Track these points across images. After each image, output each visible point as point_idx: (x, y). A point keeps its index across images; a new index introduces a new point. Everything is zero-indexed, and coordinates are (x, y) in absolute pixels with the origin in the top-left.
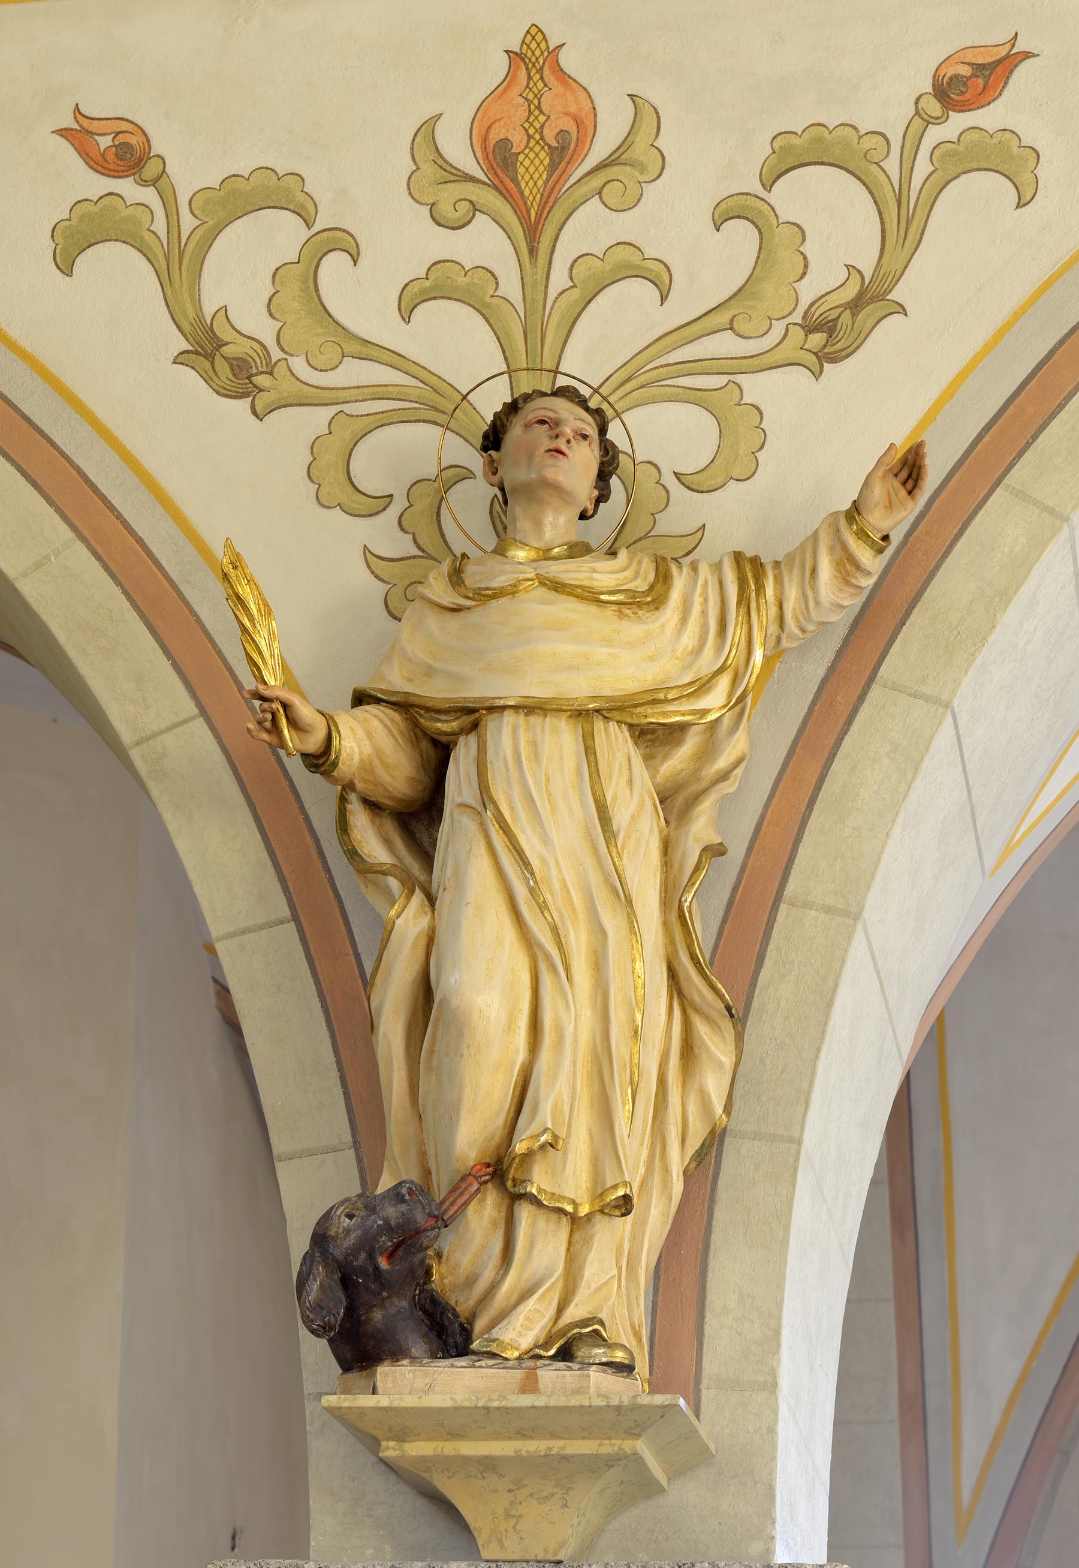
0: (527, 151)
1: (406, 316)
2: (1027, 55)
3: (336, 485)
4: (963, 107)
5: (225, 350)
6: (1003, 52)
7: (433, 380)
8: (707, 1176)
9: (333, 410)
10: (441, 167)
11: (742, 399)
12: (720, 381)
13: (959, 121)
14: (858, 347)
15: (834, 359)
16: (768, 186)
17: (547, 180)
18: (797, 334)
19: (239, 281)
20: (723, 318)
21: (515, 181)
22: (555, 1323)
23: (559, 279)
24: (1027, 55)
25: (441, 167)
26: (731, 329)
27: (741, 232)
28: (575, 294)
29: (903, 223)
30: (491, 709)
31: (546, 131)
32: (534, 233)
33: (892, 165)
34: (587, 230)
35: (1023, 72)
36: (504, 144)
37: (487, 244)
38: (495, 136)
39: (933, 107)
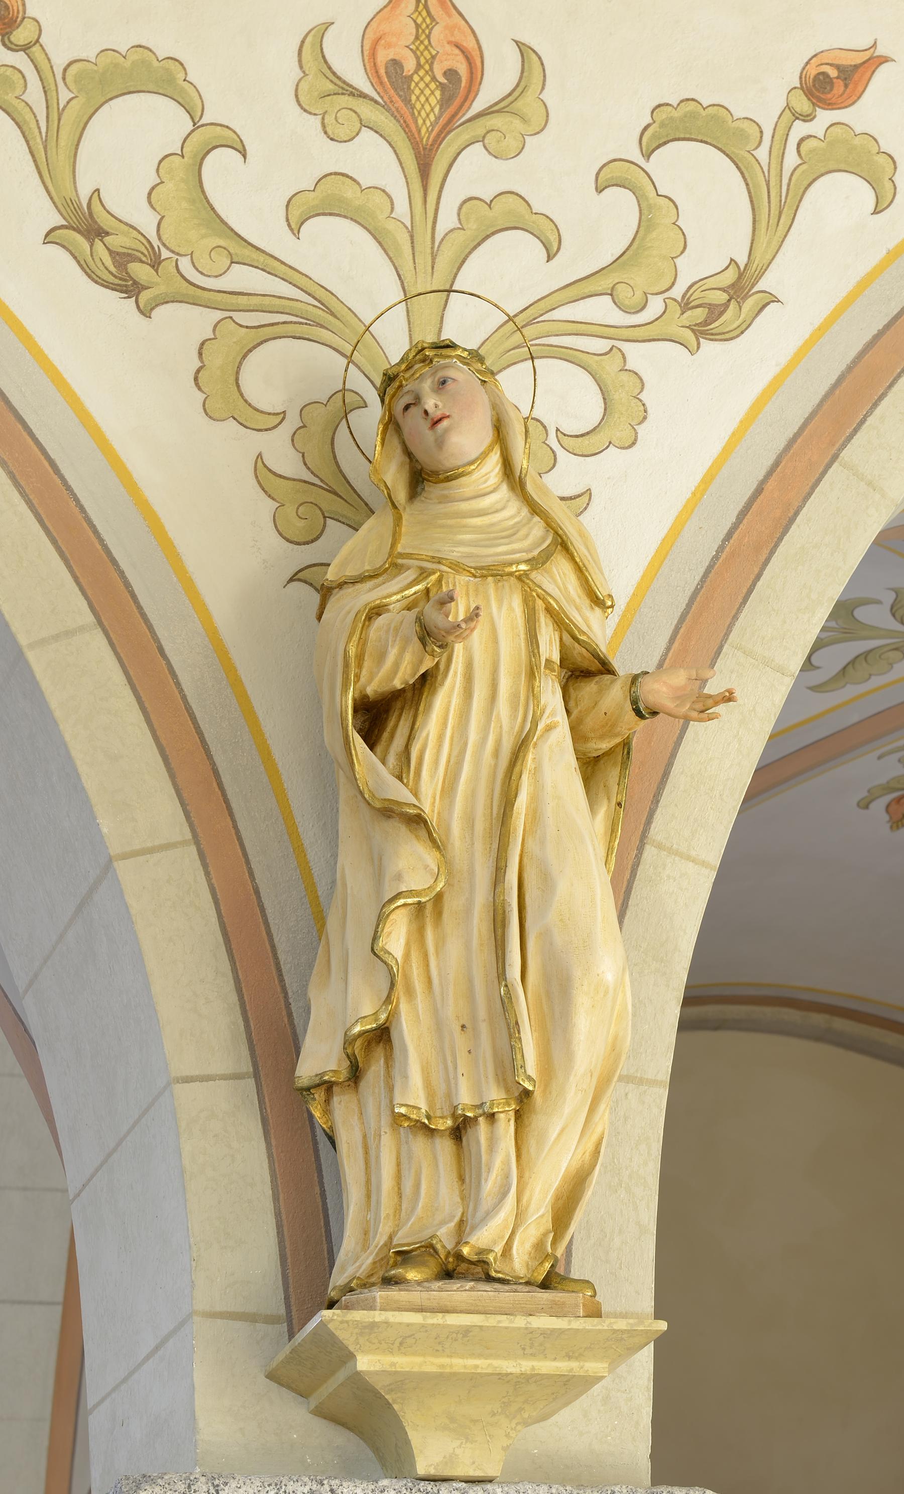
0: (418, 53)
1: (296, 231)
2: (885, 60)
3: (219, 389)
4: (830, 105)
5: (107, 239)
6: (866, 56)
7: (320, 293)
8: (602, 1165)
9: (219, 315)
10: (331, 81)
11: (625, 365)
12: (601, 345)
13: (825, 117)
14: (732, 339)
15: (713, 337)
16: (647, 156)
17: (438, 118)
18: (675, 309)
19: (125, 153)
20: (605, 283)
21: (407, 101)
22: (549, 610)
23: (447, 220)
24: (885, 60)
25: (331, 81)
26: (611, 295)
27: (622, 202)
28: (460, 236)
29: (774, 209)
30: (359, 1100)
31: (436, 67)
32: (424, 162)
33: (762, 154)
34: (472, 172)
35: (883, 74)
36: (396, 64)
37: (375, 161)
38: (383, 57)
39: (802, 104)
